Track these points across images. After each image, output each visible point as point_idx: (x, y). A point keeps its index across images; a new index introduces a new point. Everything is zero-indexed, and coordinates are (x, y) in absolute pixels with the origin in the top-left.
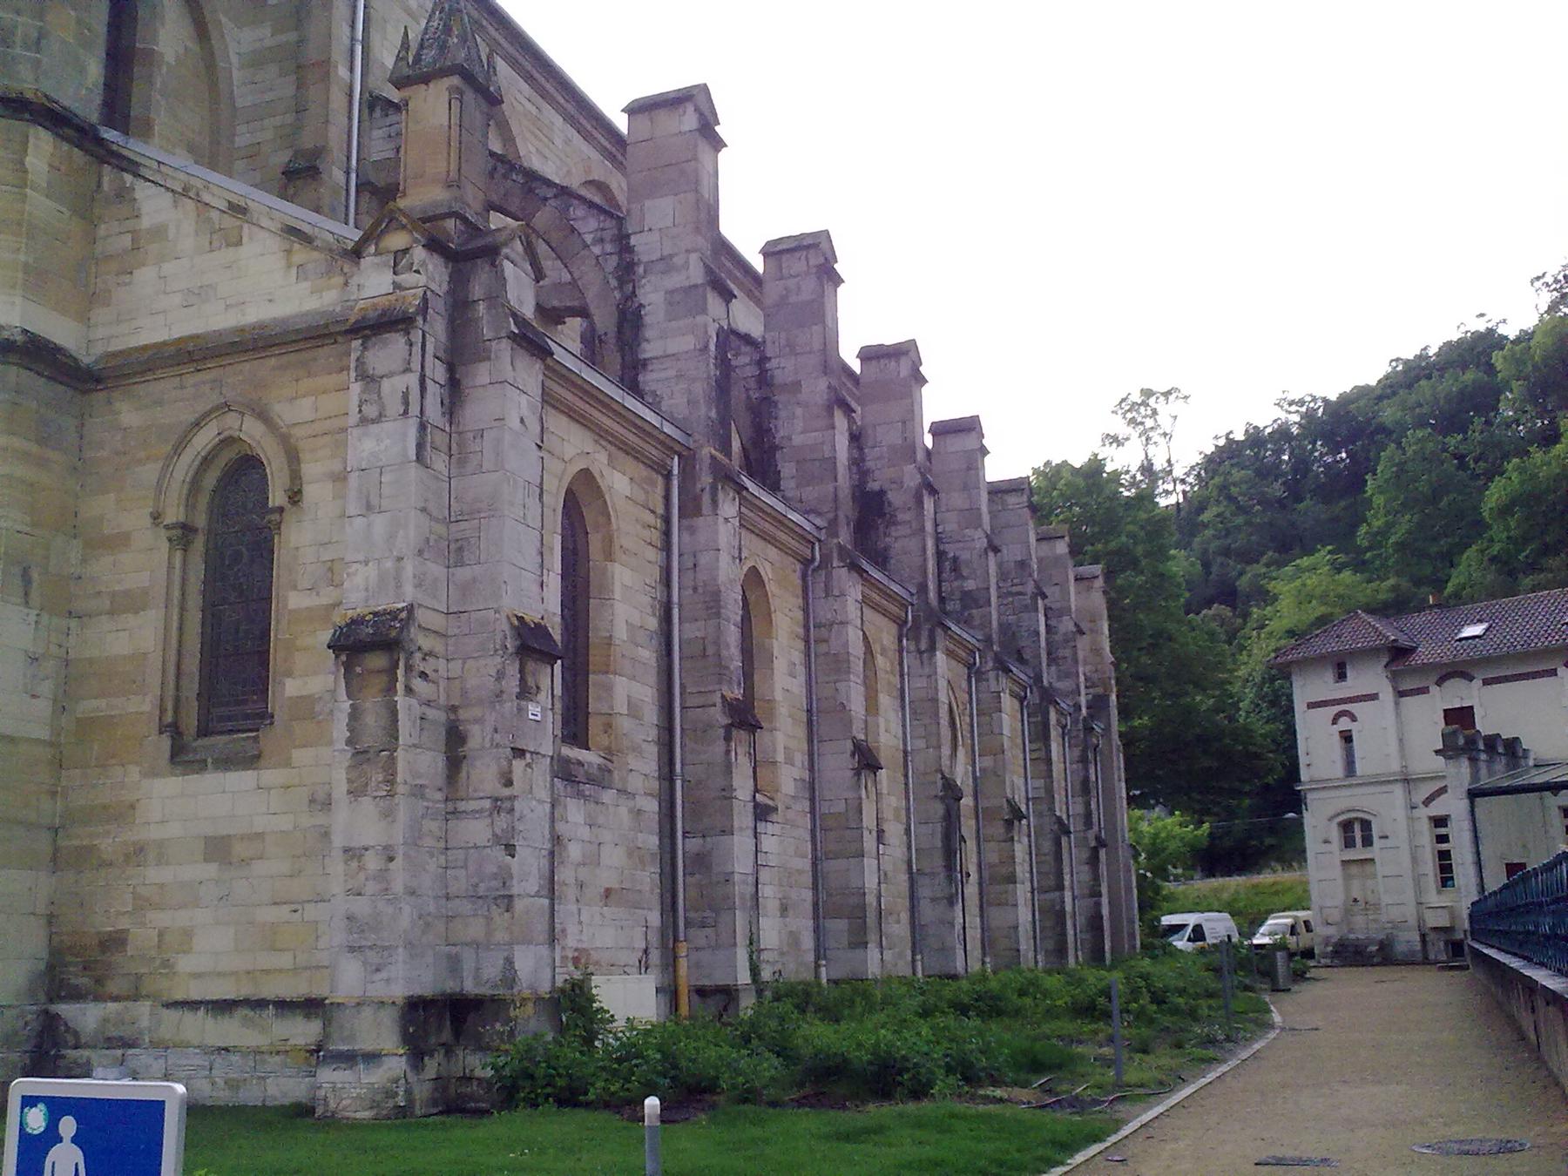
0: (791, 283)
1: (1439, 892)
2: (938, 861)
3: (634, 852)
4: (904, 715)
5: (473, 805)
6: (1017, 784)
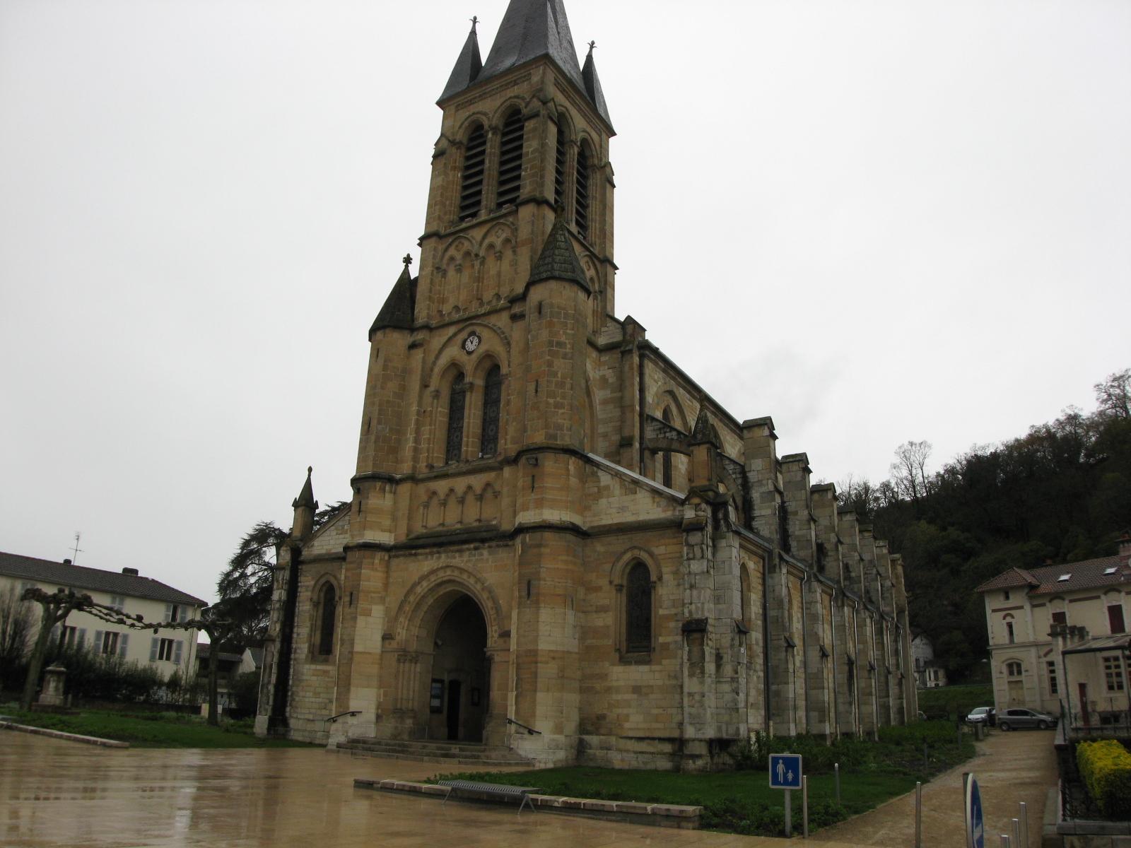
0: (792, 474)
1: (1051, 696)
2: (846, 688)
3: (758, 690)
4: (832, 631)
5: (725, 680)
6: (872, 654)
